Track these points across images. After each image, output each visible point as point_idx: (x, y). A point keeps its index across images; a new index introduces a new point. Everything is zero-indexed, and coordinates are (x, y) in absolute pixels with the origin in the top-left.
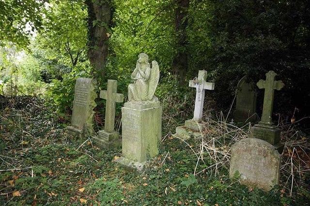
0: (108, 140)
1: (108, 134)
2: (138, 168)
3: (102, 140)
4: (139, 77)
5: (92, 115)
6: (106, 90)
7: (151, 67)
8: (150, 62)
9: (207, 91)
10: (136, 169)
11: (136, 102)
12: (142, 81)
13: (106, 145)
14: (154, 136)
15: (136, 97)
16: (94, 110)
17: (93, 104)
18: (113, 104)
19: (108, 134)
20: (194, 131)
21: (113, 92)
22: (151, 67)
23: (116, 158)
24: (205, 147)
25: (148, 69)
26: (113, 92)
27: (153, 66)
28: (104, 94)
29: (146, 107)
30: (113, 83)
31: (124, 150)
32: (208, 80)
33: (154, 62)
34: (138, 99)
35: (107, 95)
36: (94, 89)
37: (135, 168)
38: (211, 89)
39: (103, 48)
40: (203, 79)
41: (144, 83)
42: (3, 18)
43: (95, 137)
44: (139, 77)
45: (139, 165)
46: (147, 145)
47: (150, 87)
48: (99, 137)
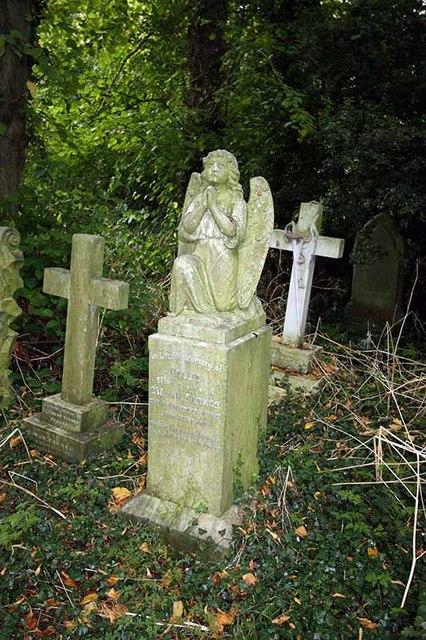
0: (78, 428)
1: (79, 411)
2: (218, 539)
3: (58, 431)
4: (210, 232)
5: (8, 343)
6: (68, 268)
7: (247, 199)
8: (244, 181)
9: (321, 263)
10: (210, 543)
11: (203, 319)
12: (219, 247)
13: (76, 445)
14: (251, 423)
15: (202, 302)
16: (11, 326)
17: (8, 310)
18: (93, 314)
19: (79, 411)
20: (289, 372)
21: (93, 276)
22: (247, 199)
23: (120, 493)
24: (387, 440)
25: (240, 204)
26: (93, 276)
27: (253, 195)
28: (55, 281)
29: (237, 333)
30: (93, 247)
31: (154, 475)
32: (327, 229)
33: (258, 184)
34: (205, 307)
35: (68, 286)
36: (13, 260)
37: (203, 537)
38: (337, 257)
39: (15, 127)
40: (313, 227)
41: (225, 254)
42: (50, 623)
43: (31, 419)
44: (210, 232)
45: (216, 526)
46: (236, 457)
47: (242, 269)
48: (46, 419)
